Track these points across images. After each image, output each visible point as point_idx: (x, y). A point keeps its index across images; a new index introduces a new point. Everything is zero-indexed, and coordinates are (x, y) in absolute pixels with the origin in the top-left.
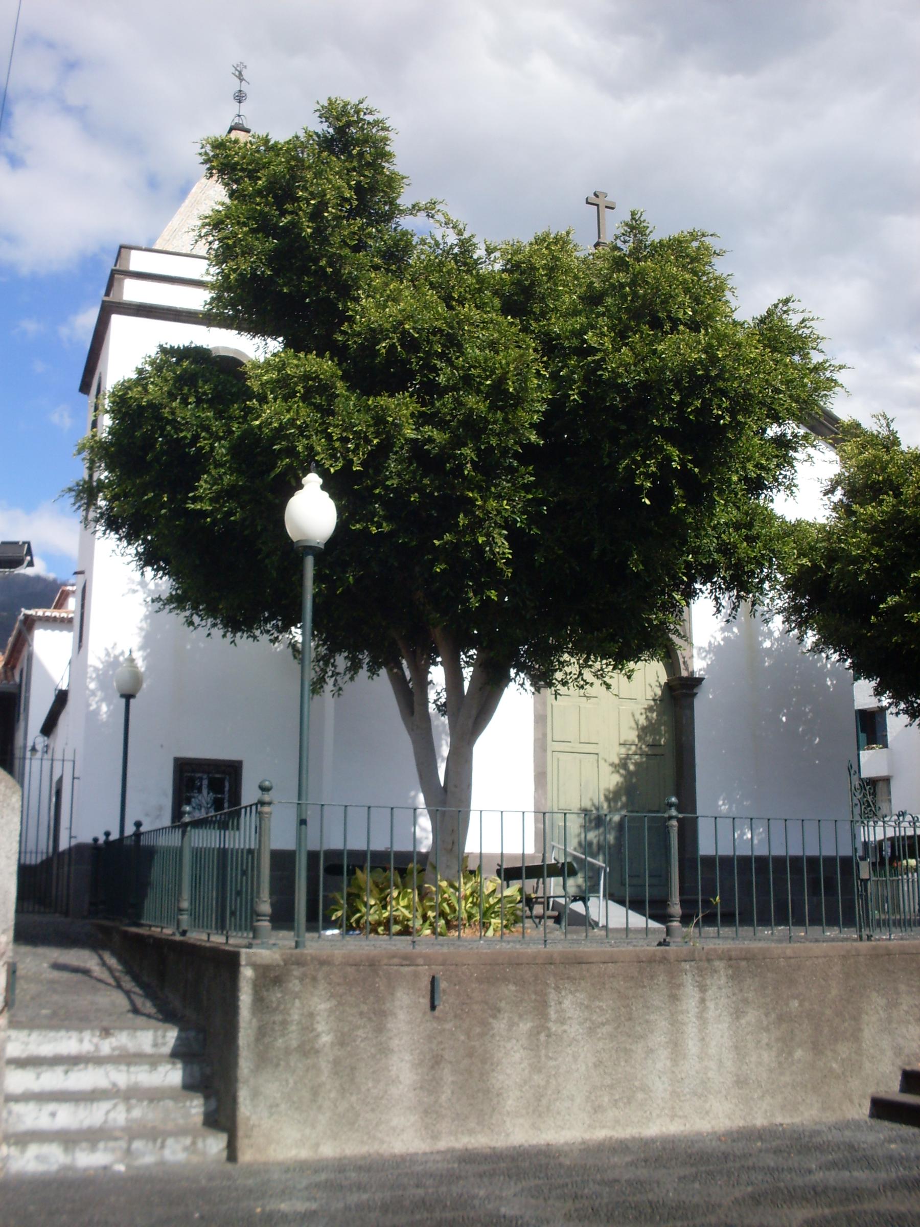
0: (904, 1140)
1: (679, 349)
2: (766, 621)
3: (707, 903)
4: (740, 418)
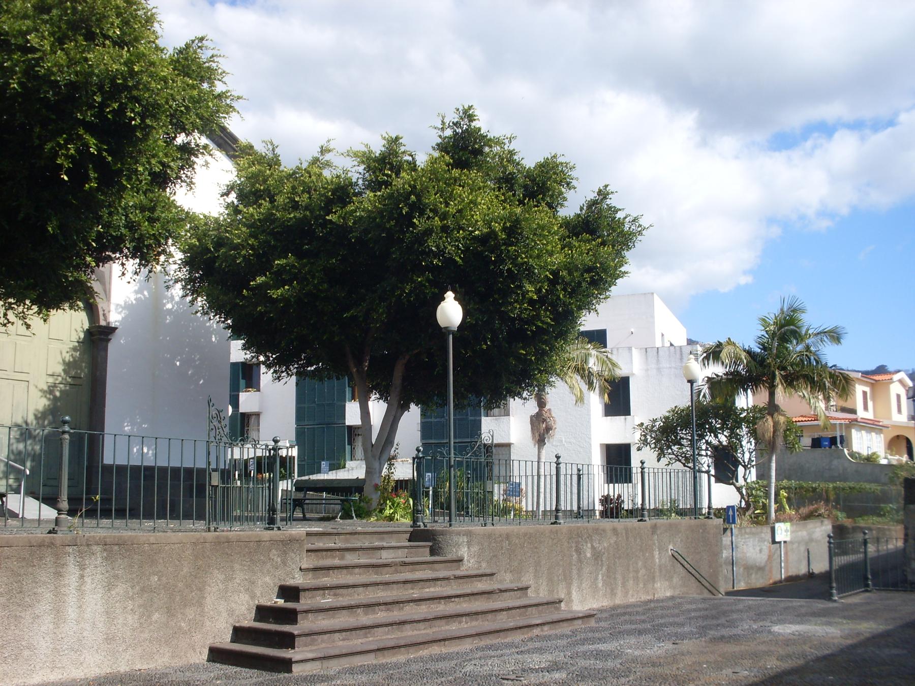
0: (228, 677)
1: (105, 60)
2: (168, 287)
3: (89, 500)
4: (148, 121)
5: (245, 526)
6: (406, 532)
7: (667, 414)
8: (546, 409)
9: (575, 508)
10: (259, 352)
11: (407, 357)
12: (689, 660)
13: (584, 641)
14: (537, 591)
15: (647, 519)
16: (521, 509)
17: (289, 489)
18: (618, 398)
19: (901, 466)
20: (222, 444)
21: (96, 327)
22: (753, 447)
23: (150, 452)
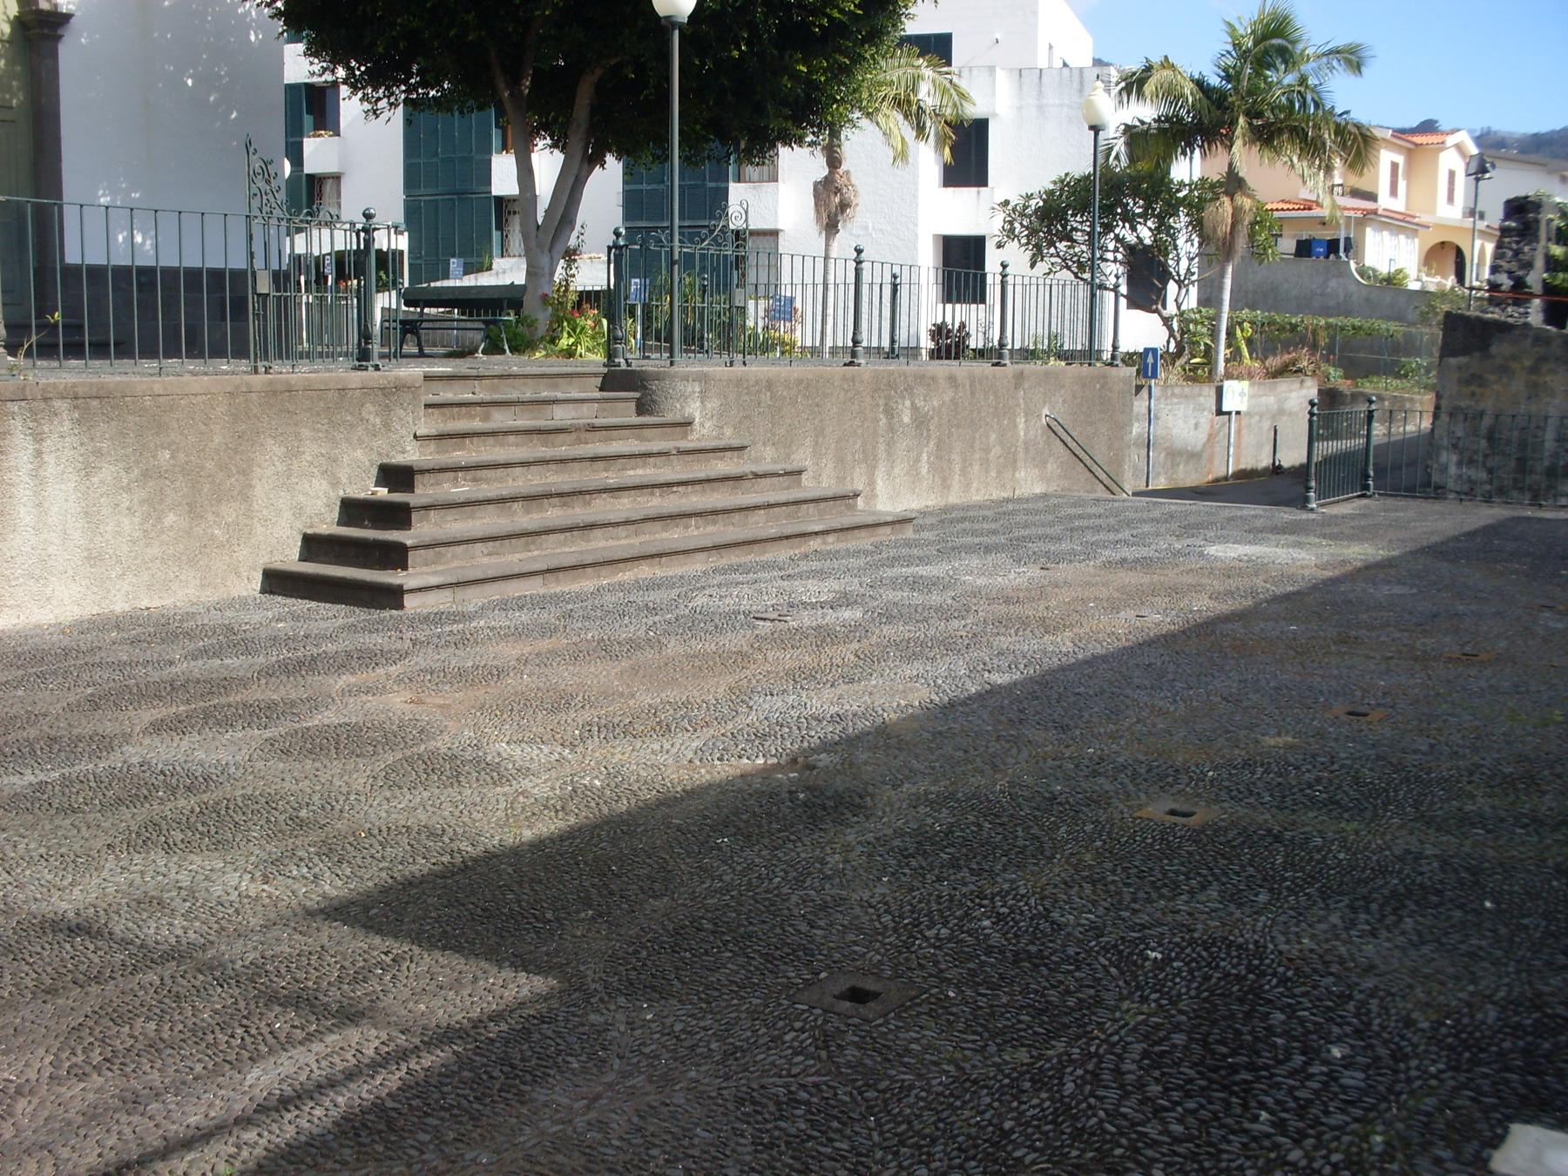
0: (295, 617)
5: (318, 365)
6: (595, 375)
7: (1052, 187)
8: (840, 171)
9: (886, 344)
10: (335, 61)
11: (598, 72)
12: (1066, 595)
13: (893, 562)
14: (817, 477)
15: (1007, 361)
16: (793, 345)
17: (394, 306)
18: (967, 156)
19: (1442, 295)
20: (274, 221)
21: (31, 12)
22: (1195, 250)
23: (148, 242)
